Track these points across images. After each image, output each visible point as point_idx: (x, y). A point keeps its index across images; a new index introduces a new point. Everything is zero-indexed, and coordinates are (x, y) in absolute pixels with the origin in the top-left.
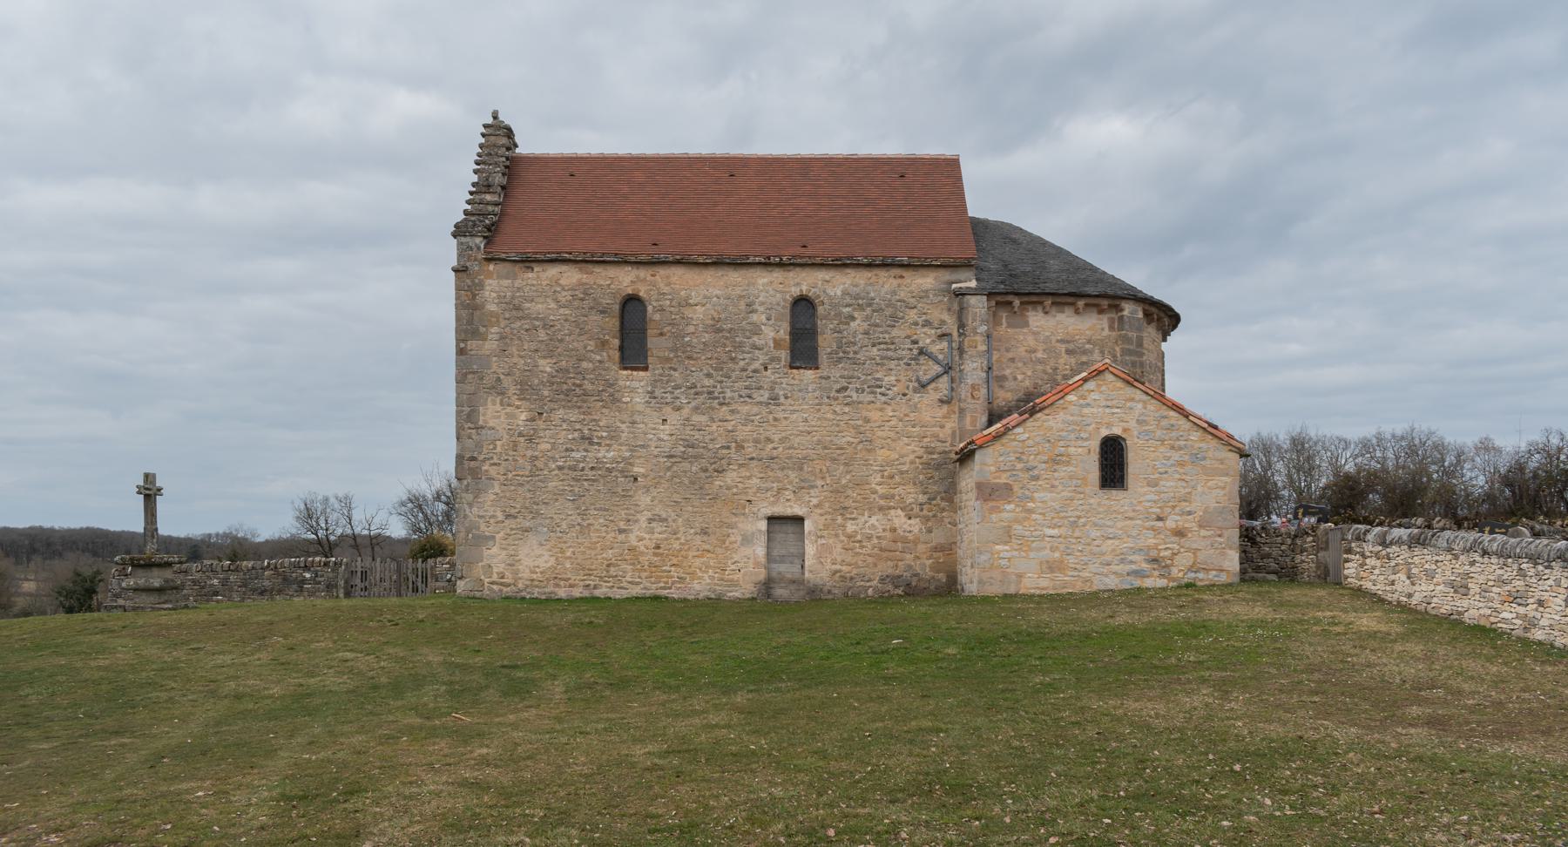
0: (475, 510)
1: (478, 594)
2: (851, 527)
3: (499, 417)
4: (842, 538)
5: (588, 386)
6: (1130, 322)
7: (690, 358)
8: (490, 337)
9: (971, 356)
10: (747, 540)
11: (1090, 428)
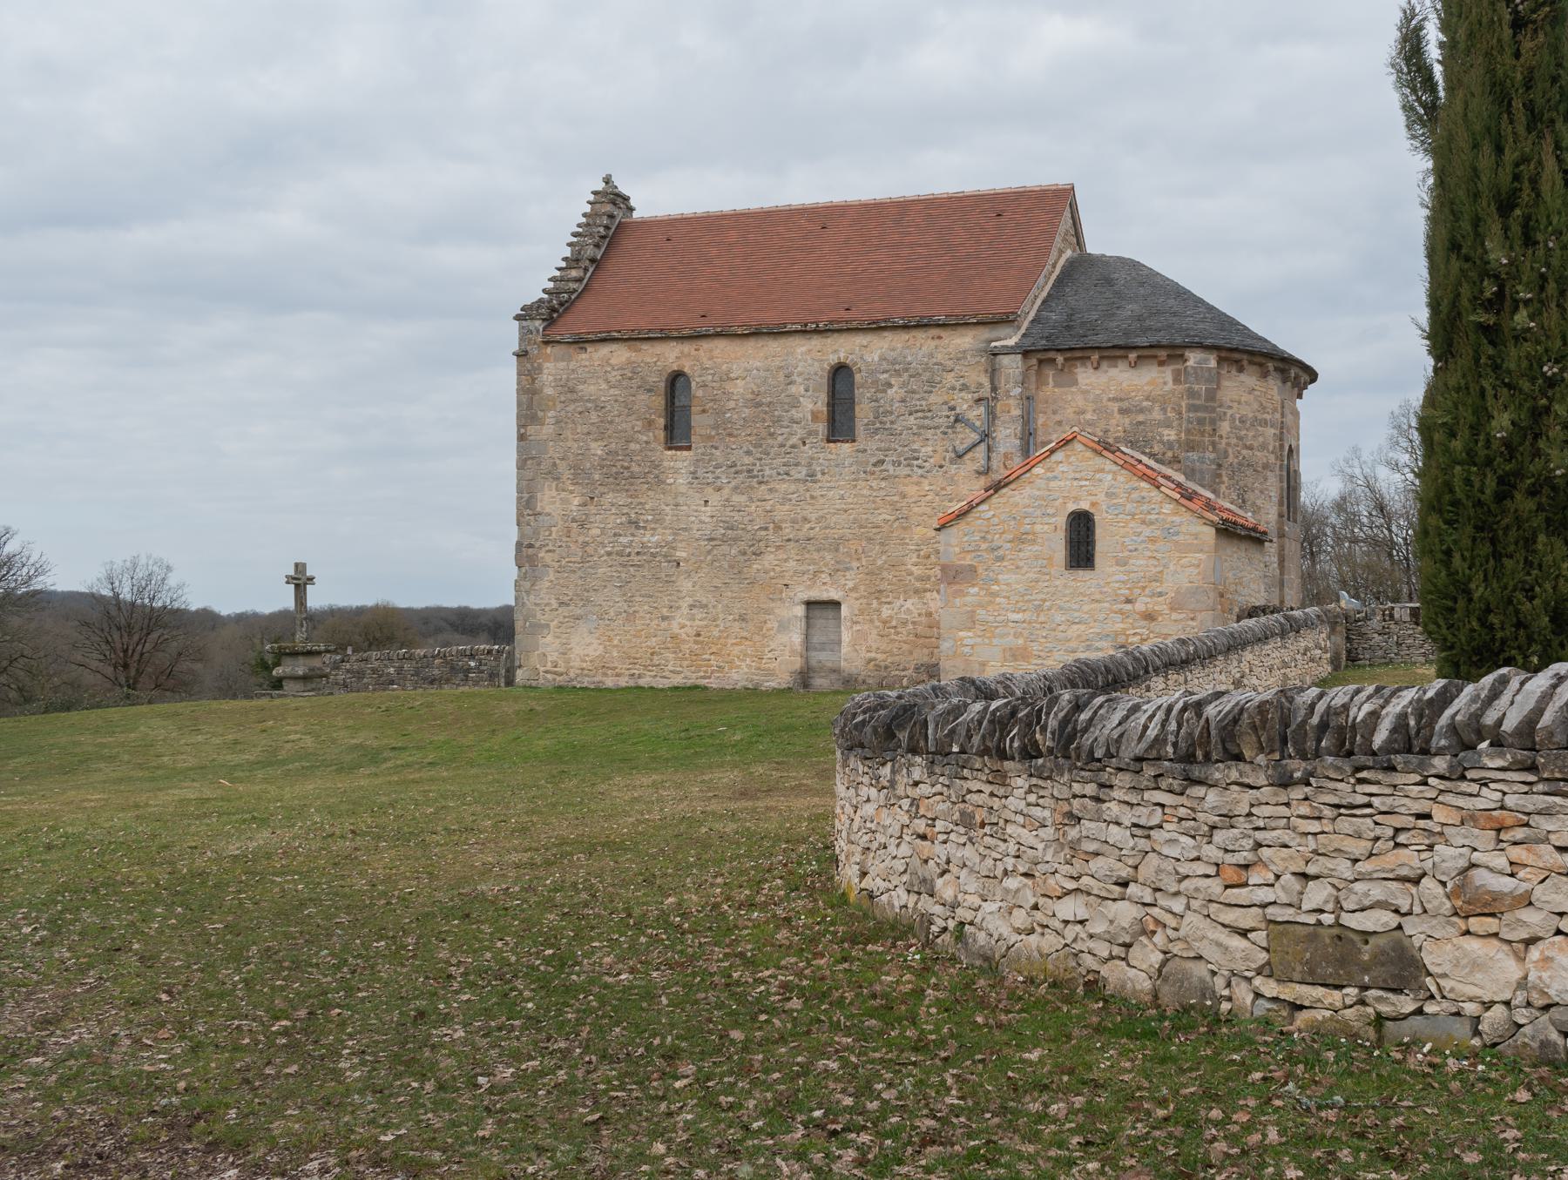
0: (532, 597)
1: (534, 683)
2: (886, 612)
3: (554, 503)
4: (877, 623)
5: (635, 469)
6: (1196, 373)
7: (730, 435)
8: (547, 421)
9: (1004, 422)
10: (783, 627)
11: (1057, 503)
